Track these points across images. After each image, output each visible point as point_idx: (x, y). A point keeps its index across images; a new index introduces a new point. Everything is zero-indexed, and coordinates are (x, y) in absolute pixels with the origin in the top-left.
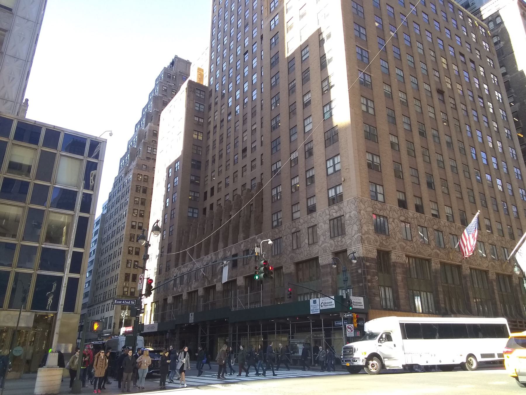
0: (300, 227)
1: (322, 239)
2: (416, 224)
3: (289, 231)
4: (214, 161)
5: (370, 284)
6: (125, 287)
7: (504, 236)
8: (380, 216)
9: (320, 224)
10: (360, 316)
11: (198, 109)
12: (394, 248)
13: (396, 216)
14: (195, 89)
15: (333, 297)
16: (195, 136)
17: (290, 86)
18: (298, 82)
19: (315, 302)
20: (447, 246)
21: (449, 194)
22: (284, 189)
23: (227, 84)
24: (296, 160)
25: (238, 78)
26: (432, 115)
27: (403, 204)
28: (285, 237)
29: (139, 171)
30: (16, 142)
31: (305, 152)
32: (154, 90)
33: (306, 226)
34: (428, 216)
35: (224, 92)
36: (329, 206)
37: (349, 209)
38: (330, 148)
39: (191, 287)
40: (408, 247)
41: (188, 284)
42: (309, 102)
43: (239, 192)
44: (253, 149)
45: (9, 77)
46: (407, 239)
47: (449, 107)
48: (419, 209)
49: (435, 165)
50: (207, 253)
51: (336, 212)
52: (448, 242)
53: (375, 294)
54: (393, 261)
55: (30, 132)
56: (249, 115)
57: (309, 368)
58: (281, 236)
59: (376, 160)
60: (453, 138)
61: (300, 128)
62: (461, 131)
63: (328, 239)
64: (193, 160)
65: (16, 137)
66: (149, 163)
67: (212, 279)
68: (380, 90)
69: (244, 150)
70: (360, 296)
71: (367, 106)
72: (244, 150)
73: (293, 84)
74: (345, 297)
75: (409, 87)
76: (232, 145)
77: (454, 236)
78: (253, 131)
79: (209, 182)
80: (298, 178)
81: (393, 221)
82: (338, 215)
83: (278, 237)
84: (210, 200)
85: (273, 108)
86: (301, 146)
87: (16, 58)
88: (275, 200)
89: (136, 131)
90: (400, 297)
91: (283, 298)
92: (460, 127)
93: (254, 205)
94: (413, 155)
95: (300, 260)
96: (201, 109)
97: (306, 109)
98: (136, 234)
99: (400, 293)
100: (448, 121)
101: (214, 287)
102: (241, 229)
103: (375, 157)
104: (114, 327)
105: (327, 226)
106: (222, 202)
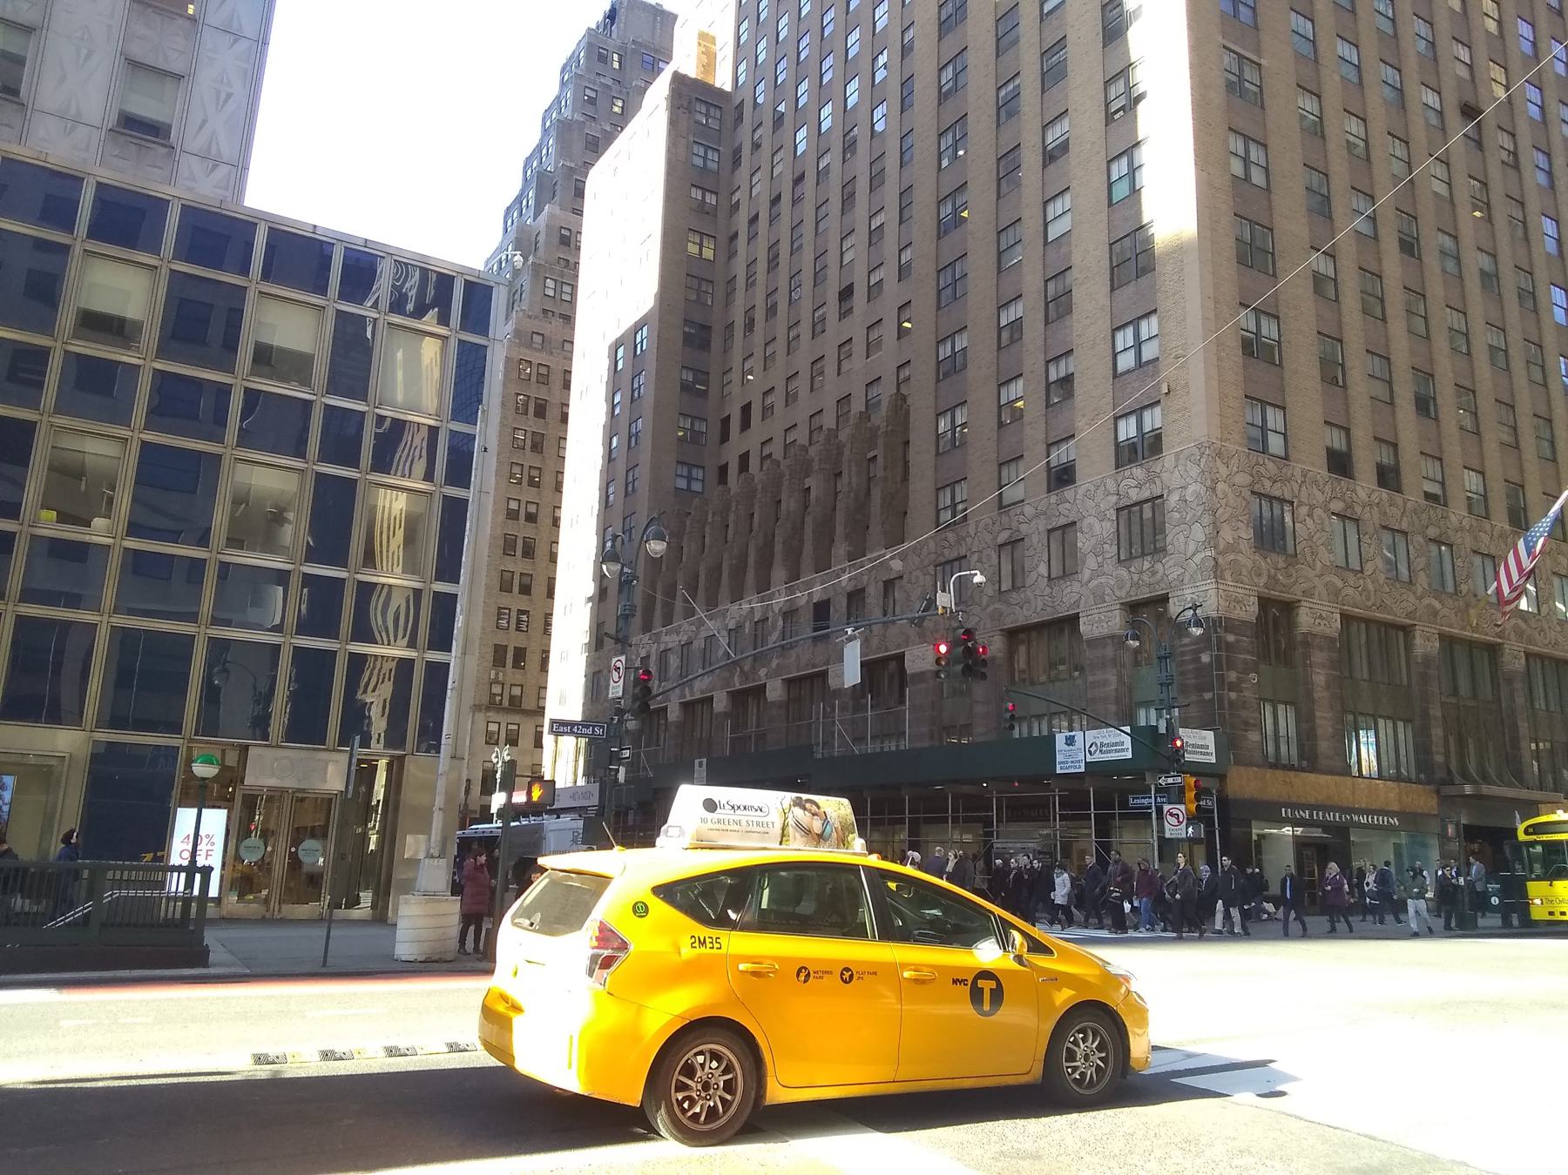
0: (1024, 528)
1: (1091, 563)
2: (1377, 522)
3: (988, 537)
4: (750, 325)
5: (1233, 695)
6: (496, 681)
7: (1487, 517)
8: (1271, 498)
9: (1086, 522)
10: (1204, 783)
11: (699, 162)
12: (1308, 593)
13: (1320, 498)
14: (692, 98)
15: (1127, 729)
16: (693, 249)
17: (1003, 93)
18: (1029, 82)
19: (1070, 741)
20: (1464, 588)
21: (1478, 433)
22: (974, 418)
23: (790, 85)
24: (1017, 325)
25: (826, 65)
26: (1441, 189)
27: (1340, 463)
28: (975, 557)
29: (523, 350)
30: (94, 246)
31: (1047, 304)
32: (558, 99)
33: (1042, 525)
34: (1413, 497)
35: (782, 108)
36: (1117, 467)
37: (1180, 478)
38: (1127, 292)
39: (691, 689)
40: (1350, 591)
41: (685, 680)
42: (1064, 147)
43: (829, 421)
44: (874, 290)
45: (218, 92)
46: (1347, 568)
47: (1495, 158)
48: (1388, 477)
49: (1441, 343)
50: (737, 597)
51: (1139, 486)
52: (1468, 577)
53: (1246, 723)
54: (1304, 629)
55: (302, 257)
56: (862, 185)
57: (1100, 921)
58: (962, 553)
59: (1269, 329)
60: (1501, 258)
61: (1029, 229)
62: (1527, 239)
63: (1109, 566)
64: (687, 322)
65: (95, 232)
66: (553, 327)
67: (753, 667)
68: (1287, 107)
69: (846, 293)
70: (1204, 726)
71: (1246, 161)
72: (846, 293)
73: (1011, 87)
74: (1162, 730)
75: (1377, 100)
76: (807, 277)
77: (1398, 537)
78: (875, 235)
79: (735, 388)
80: (1020, 382)
81: (1310, 515)
82: (1146, 494)
83: (955, 555)
84: (739, 443)
85: (945, 163)
86: (1032, 281)
88: (952, 447)
89: (506, 230)
90: (1319, 732)
91: (966, 729)
92: (1524, 223)
93: (880, 460)
94: (1378, 313)
95: (1022, 621)
97: (1051, 167)
98: (521, 536)
99: (1318, 721)
100: (1488, 204)
101: (762, 689)
102: (840, 530)
103: (1264, 322)
105: (1108, 528)
106: (776, 449)
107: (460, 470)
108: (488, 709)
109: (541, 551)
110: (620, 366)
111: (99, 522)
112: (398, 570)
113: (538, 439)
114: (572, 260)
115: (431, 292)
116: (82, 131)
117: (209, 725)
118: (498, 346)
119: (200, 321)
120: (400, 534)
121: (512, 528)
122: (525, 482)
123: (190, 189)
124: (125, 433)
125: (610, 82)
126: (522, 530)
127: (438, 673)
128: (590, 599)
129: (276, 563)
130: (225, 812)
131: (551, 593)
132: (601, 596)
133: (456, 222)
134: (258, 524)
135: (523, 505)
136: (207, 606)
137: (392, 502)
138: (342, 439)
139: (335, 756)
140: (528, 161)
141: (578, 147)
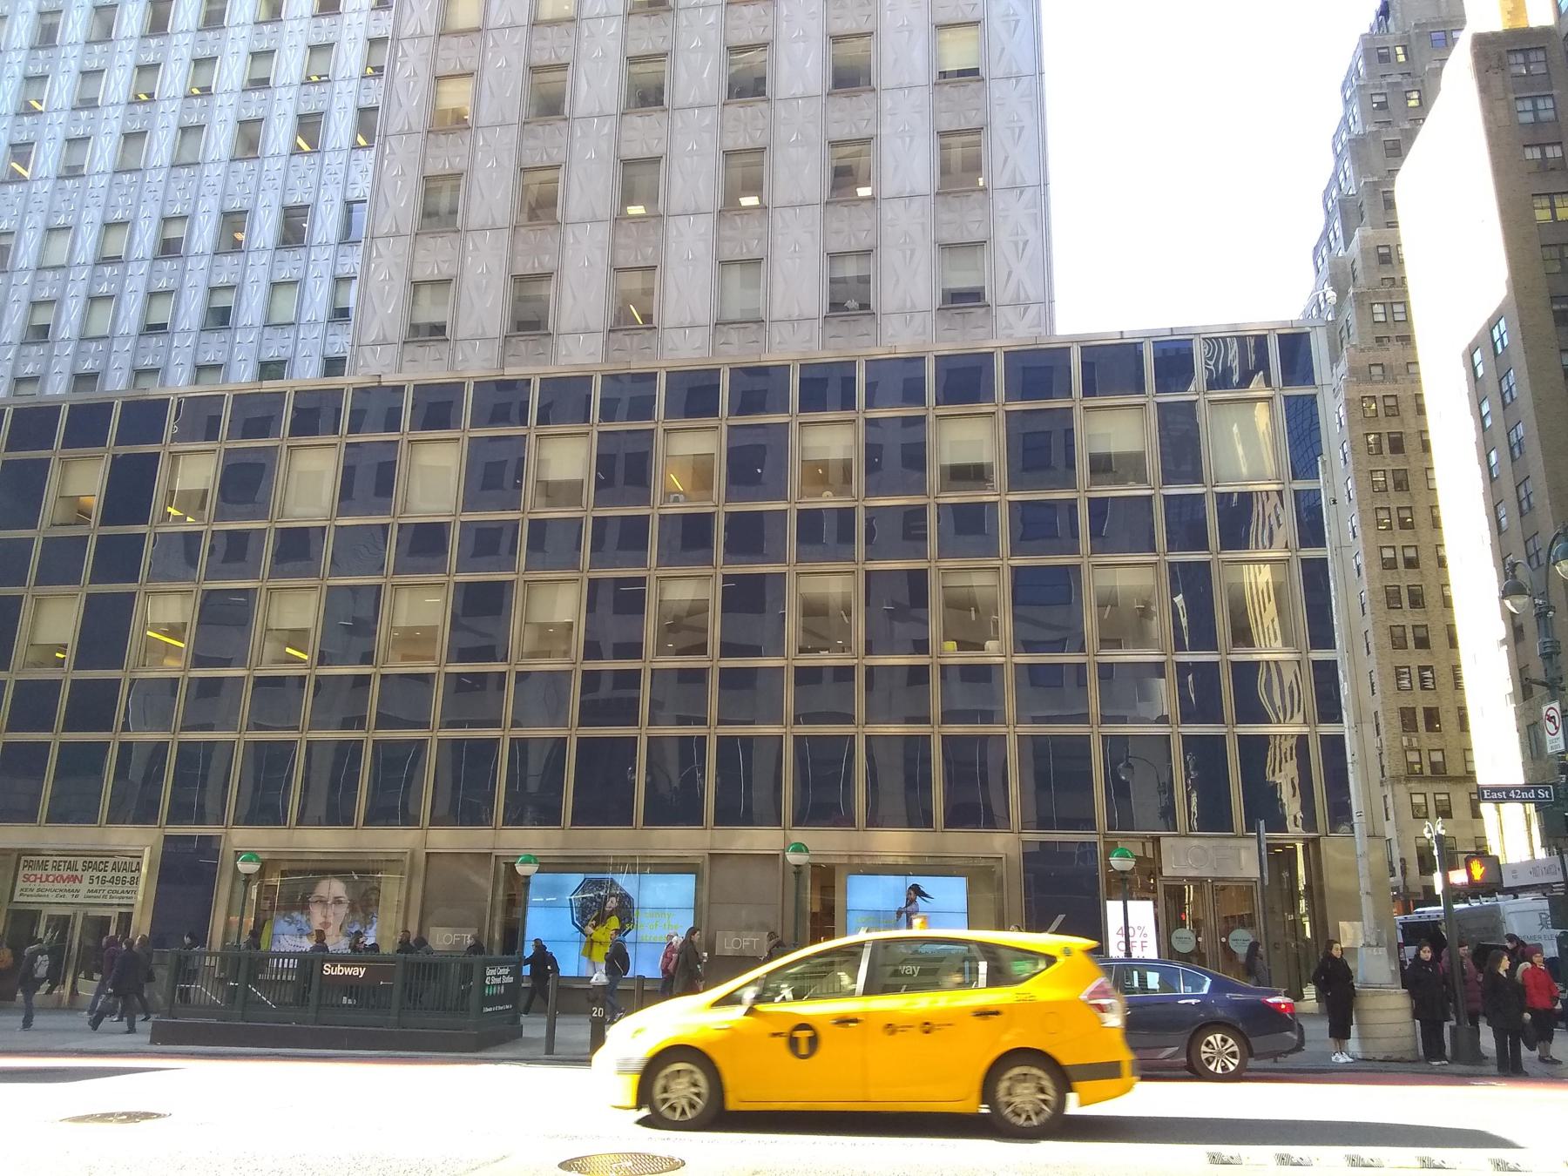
16: (1543, 215)
29: (1362, 387)
32: (1345, 120)
45: (1016, 244)
55: (1112, 366)
64: (1554, 299)
87: (1016, 188)
96: (1543, 115)
98: (1404, 585)
104: (1404, 872)
107: (1311, 528)
108: (1408, 780)
109: (1431, 597)
110: (1480, 372)
111: (990, 645)
112: (1279, 643)
113: (1400, 476)
114: (1398, 277)
115: (1252, 357)
116: (918, 318)
117: (1122, 819)
118: (1328, 392)
119: (1040, 449)
120: (1271, 607)
121: (1391, 579)
122: (1396, 526)
123: (1010, 336)
124: (997, 563)
125: (1398, 79)
126: (1405, 579)
127: (1334, 746)
128: (1503, 642)
129: (1151, 656)
130: (1150, 904)
131: (1453, 642)
132: (1517, 633)
133: (1265, 279)
134: (1126, 623)
135: (1399, 552)
136: (1094, 707)
137: (1257, 576)
138: (1186, 524)
139: (1245, 842)
140: (1327, 193)
141: (1377, 157)
